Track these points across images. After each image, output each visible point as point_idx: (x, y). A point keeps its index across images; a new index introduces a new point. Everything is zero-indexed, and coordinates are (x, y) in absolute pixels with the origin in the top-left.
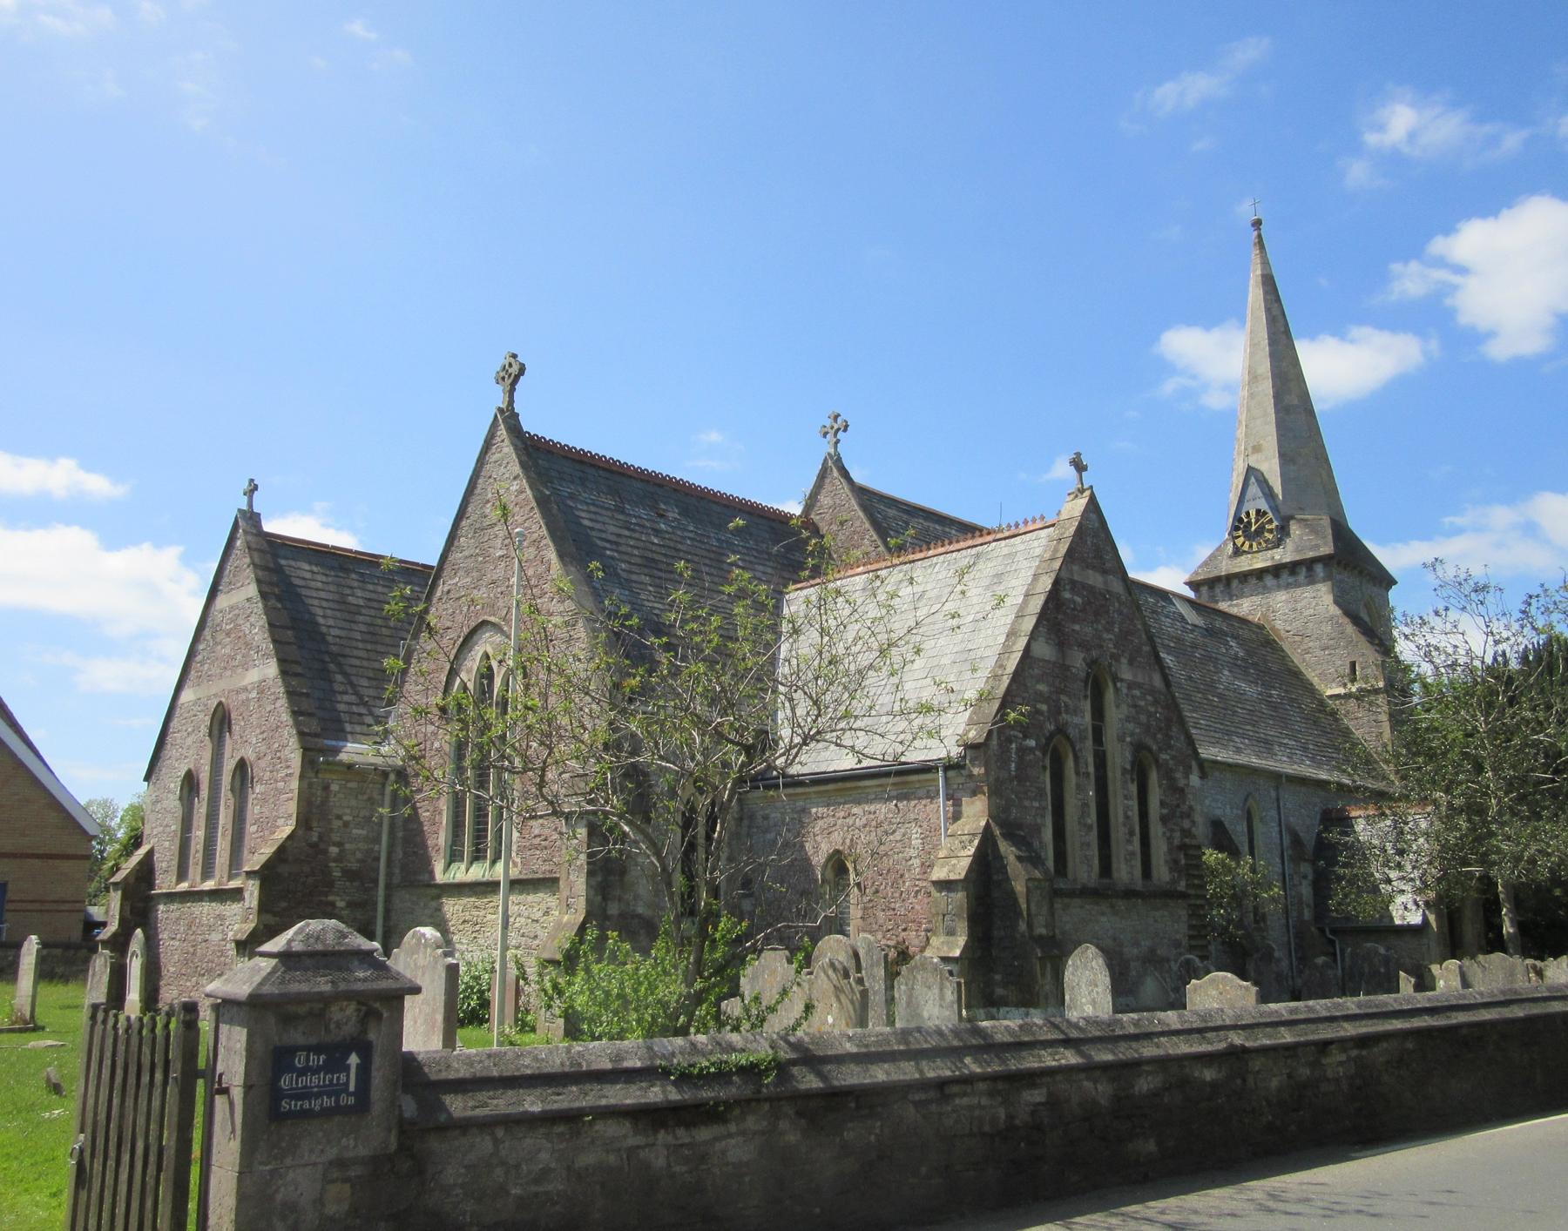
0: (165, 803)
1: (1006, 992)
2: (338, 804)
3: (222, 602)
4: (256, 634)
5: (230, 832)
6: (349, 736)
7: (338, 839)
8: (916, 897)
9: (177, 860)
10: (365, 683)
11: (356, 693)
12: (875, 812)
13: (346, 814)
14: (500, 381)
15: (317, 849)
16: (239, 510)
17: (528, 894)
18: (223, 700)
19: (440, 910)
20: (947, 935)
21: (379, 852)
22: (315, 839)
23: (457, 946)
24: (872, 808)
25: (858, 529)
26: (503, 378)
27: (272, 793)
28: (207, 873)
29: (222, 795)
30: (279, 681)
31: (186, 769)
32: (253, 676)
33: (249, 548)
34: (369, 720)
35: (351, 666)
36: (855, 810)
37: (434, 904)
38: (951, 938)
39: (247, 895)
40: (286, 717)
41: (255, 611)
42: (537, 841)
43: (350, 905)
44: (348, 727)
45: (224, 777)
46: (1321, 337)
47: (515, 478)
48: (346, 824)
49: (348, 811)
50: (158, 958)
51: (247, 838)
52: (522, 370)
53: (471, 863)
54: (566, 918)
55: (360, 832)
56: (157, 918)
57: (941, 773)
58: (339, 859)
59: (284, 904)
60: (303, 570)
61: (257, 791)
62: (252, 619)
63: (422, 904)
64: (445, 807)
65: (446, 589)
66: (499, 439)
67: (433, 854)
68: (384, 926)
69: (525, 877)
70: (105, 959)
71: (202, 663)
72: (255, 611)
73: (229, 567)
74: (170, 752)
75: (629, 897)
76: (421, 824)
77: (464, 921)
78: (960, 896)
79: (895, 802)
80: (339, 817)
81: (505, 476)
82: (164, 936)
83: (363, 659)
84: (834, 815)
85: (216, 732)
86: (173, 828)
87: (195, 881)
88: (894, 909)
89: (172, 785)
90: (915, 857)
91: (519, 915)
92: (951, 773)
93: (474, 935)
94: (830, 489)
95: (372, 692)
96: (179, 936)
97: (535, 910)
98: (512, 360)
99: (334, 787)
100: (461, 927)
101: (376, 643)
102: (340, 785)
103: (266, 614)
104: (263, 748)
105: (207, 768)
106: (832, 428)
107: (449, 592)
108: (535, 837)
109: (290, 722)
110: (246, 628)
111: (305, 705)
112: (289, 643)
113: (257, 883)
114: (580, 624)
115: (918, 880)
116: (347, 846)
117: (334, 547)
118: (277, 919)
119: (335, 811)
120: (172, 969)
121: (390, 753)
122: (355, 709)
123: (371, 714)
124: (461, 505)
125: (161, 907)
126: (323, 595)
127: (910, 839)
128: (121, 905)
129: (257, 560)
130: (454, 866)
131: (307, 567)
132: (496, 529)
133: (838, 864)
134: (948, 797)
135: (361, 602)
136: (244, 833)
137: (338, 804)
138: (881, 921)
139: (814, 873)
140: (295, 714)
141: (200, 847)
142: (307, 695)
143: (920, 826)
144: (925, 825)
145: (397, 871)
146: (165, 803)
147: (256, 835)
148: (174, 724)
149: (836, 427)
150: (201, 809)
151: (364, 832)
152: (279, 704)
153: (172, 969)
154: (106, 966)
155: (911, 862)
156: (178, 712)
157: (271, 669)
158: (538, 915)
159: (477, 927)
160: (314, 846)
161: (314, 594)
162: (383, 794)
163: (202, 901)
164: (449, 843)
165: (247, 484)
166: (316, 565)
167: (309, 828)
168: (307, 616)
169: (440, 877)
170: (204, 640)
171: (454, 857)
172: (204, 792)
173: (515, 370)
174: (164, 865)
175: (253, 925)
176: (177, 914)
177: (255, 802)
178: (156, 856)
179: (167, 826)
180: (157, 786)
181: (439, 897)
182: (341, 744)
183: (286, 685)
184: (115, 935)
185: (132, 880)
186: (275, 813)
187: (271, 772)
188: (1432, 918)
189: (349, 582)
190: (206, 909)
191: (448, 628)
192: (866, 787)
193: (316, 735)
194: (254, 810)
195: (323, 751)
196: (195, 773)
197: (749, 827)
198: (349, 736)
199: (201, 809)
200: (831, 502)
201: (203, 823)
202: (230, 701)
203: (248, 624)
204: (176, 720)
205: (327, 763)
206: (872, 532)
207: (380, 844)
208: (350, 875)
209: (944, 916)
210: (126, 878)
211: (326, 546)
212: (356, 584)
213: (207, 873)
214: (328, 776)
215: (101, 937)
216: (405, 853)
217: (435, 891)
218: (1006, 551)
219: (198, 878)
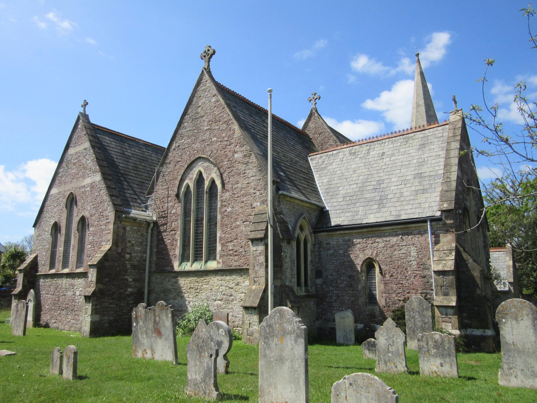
0: (43, 237)
1: (470, 322)
2: (129, 236)
3: (71, 151)
4: (89, 163)
5: (76, 248)
6: (132, 207)
7: (129, 251)
8: (414, 278)
9: (49, 260)
10: (135, 186)
11: (133, 190)
12: (389, 241)
13: (133, 241)
14: (203, 58)
15: (121, 255)
16: (80, 112)
17: (227, 276)
18: (73, 192)
19: (177, 283)
20: (444, 295)
21: (146, 258)
22: (120, 251)
23: (187, 299)
24: (388, 239)
25: (327, 136)
26: (205, 56)
27: (99, 230)
28: (65, 265)
29: (73, 232)
30: (102, 182)
31: (54, 221)
32: (88, 181)
33: (85, 127)
34: (139, 201)
35: (130, 179)
36: (378, 240)
37: (174, 280)
38: (447, 297)
39: (90, 275)
40: (106, 198)
41: (89, 153)
42: (231, 252)
43: (134, 280)
44: (132, 204)
45: (73, 224)
46: (360, 121)
47: (214, 96)
48: (133, 245)
49: (133, 239)
50: (40, 302)
51: (85, 251)
52: (214, 52)
53: (193, 262)
54: (254, 287)
55: (138, 248)
56: (39, 285)
57: (429, 223)
58: (130, 260)
59: (107, 280)
60: (107, 140)
61: (91, 230)
62: (87, 157)
63: (167, 280)
64: (179, 238)
65: (177, 145)
66: (203, 81)
67: (173, 258)
68: (148, 290)
69: (225, 268)
70: (23, 304)
71: (61, 177)
72: (89, 153)
73: (75, 136)
74: (45, 214)
75: (283, 278)
76: (166, 246)
77: (191, 288)
78: (451, 278)
79: (400, 236)
80: (130, 242)
81: (208, 96)
82: (43, 293)
83: (134, 177)
84: (366, 243)
85: (69, 206)
86: (47, 247)
87: (58, 269)
88: (402, 284)
89: (47, 229)
90: (414, 261)
91: (222, 285)
92: (433, 223)
93: (196, 294)
94: (314, 121)
95: (138, 190)
96: (50, 293)
97: (230, 283)
98: (209, 48)
99: (128, 229)
100: (189, 291)
101: (138, 171)
102: (130, 228)
103: (95, 154)
104: (94, 212)
105: (65, 221)
106: (314, 98)
107: (179, 146)
108: (230, 250)
109: (108, 199)
110: (84, 161)
111: (115, 192)
112: (105, 167)
113: (95, 270)
114: (253, 155)
115: (416, 271)
116: (133, 254)
117: (117, 132)
118: (104, 286)
119: (128, 239)
120: (47, 307)
121: (151, 215)
122: (133, 196)
123: (139, 199)
124: (185, 110)
125: (42, 280)
126: (115, 150)
127: (410, 252)
128: (23, 279)
129: (89, 132)
130: (184, 264)
131: (108, 138)
132: (204, 118)
133: (369, 264)
134: (432, 234)
135: (130, 155)
136: (84, 248)
137: (129, 236)
138: (394, 289)
139: (356, 267)
140: (111, 196)
141: (61, 255)
142: (115, 189)
143: (416, 247)
144: (419, 246)
145: (154, 265)
146: (43, 237)
147: (91, 249)
148: (48, 203)
149: (315, 98)
150: (61, 239)
151: (140, 249)
152: (102, 192)
153: (47, 307)
154: (24, 307)
155: (411, 263)
156: (49, 198)
157: (98, 177)
158: (233, 285)
159: (198, 291)
160: (119, 254)
161: (112, 149)
162: (147, 233)
163: (62, 277)
164: (181, 253)
165: (83, 102)
166: (112, 138)
167: (118, 246)
168: (110, 158)
169: (177, 267)
170: (63, 167)
171: (184, 258)
172: (63, 231)
173: (211, 52)
174: (43, 262)
175: (93, 289)
176: (50, 283)
177: (90, 235)
178: (39, 258)
179: (44, 246)
180: (39, 229)
181: (176, 277)
182: (130, 210)
183: (106, 183)
184: (20, 292)
185: (28, 269)
186: (100, 239)
187: (98, 221)
188: (512, 288)
189: (125, 147)
190: (64, 282)
191: (179, 161)
192: (384, 230)
193: (120, 205)
194: (89, 238)
195: (124, 212)
196: (58, 223)
197: (319, 248)
198: (132, 207)
199: (61, 239)
200: (314, 126)
201: (62, 244)
202: (76, 192)
203: (85, 160)
204: (48, 201)
205: (126, 218)
206: (334, 137)
207: (146, 253)
208: (134, 267)
209: (441, 287)
210: (25, 268)
211: (115, 132)
212: (127, 147)
213: (65, 265)
214: (125, 223)
215: (13, 293)
216: (157, 258)
217: (173, 275)
218: (421, 136)
219: (60, 268)
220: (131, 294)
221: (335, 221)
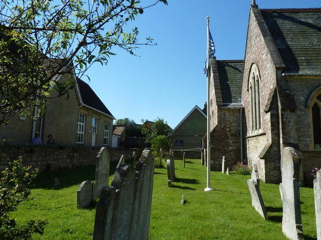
43: (233, 142)
48: (231, 123)
99: (227, 114)
160: (223, 128)
208: (233, 135)
220: (232, 150)
221: (173, 124)
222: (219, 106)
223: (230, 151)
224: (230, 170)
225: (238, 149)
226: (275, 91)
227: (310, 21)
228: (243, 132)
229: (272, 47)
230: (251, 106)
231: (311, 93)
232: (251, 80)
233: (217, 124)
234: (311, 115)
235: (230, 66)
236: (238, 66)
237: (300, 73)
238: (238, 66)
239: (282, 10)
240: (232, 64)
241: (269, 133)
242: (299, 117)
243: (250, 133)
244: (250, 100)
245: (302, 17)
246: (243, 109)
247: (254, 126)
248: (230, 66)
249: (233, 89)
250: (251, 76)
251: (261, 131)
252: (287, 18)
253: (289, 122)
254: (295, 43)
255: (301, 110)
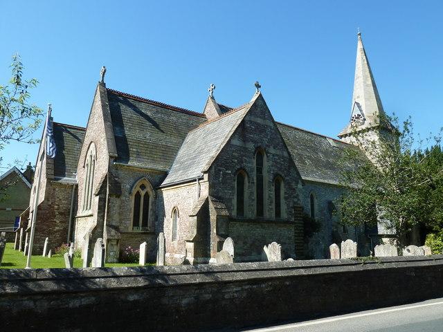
48: (60, 200)
208: (61, 214)
222: (49, 180)
223: (56, 232)
224: (53, 253)
225: (65, 230)
226: (106, 177)
227: (149, 114)
228: (73, 211)
229: (110, 133)
230: (84, 184)
231: (136, 182)
232: (88, 158)
233: (43, 199)
234: (133, 202)
235: (69, 132)
236: (78, 134)
237: (129, 163)
238: (78, 134)
239: (128, 95)
240: (72, 131)
241: (95, 218)
242: (123, 202)
243: (80, 213)
244: (84, 177)
245: (143, 108)
246: (77, 186)
247: (85, 207)
248: (69, 132)
249: (68, 160)
250: (89, 154)
251: (90, 212)
252: (131, 105)
253: (114, 206)
254: (132, 134)
255: (126, 197)
